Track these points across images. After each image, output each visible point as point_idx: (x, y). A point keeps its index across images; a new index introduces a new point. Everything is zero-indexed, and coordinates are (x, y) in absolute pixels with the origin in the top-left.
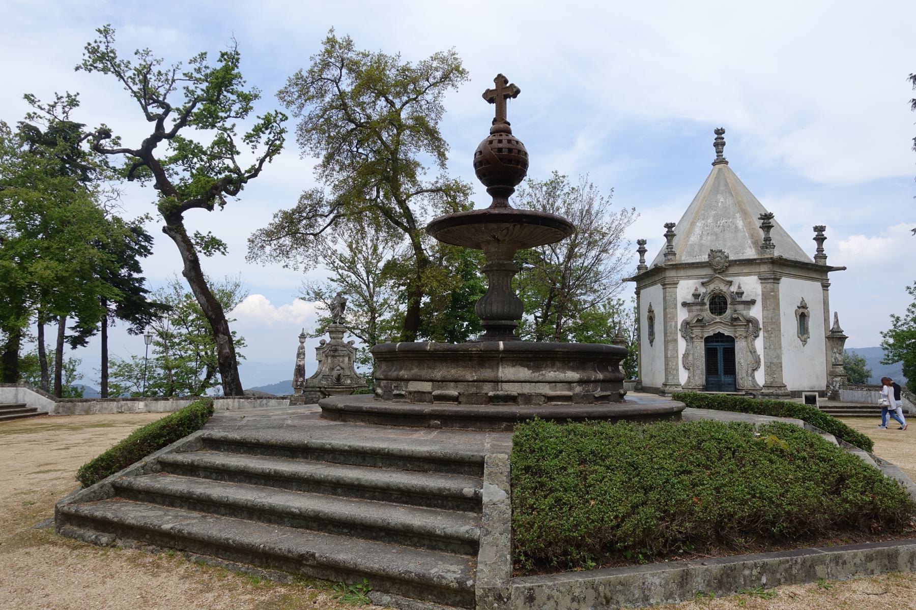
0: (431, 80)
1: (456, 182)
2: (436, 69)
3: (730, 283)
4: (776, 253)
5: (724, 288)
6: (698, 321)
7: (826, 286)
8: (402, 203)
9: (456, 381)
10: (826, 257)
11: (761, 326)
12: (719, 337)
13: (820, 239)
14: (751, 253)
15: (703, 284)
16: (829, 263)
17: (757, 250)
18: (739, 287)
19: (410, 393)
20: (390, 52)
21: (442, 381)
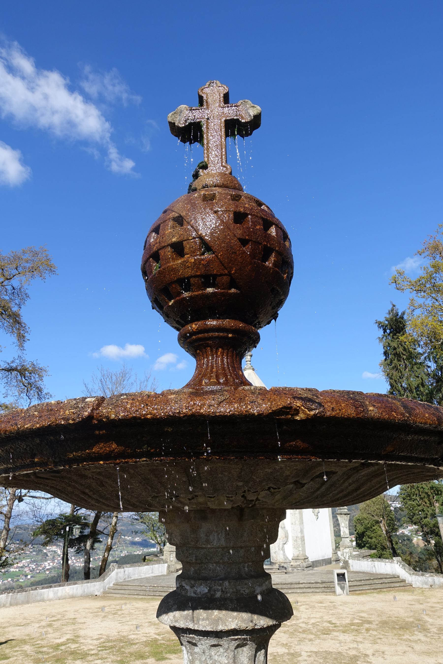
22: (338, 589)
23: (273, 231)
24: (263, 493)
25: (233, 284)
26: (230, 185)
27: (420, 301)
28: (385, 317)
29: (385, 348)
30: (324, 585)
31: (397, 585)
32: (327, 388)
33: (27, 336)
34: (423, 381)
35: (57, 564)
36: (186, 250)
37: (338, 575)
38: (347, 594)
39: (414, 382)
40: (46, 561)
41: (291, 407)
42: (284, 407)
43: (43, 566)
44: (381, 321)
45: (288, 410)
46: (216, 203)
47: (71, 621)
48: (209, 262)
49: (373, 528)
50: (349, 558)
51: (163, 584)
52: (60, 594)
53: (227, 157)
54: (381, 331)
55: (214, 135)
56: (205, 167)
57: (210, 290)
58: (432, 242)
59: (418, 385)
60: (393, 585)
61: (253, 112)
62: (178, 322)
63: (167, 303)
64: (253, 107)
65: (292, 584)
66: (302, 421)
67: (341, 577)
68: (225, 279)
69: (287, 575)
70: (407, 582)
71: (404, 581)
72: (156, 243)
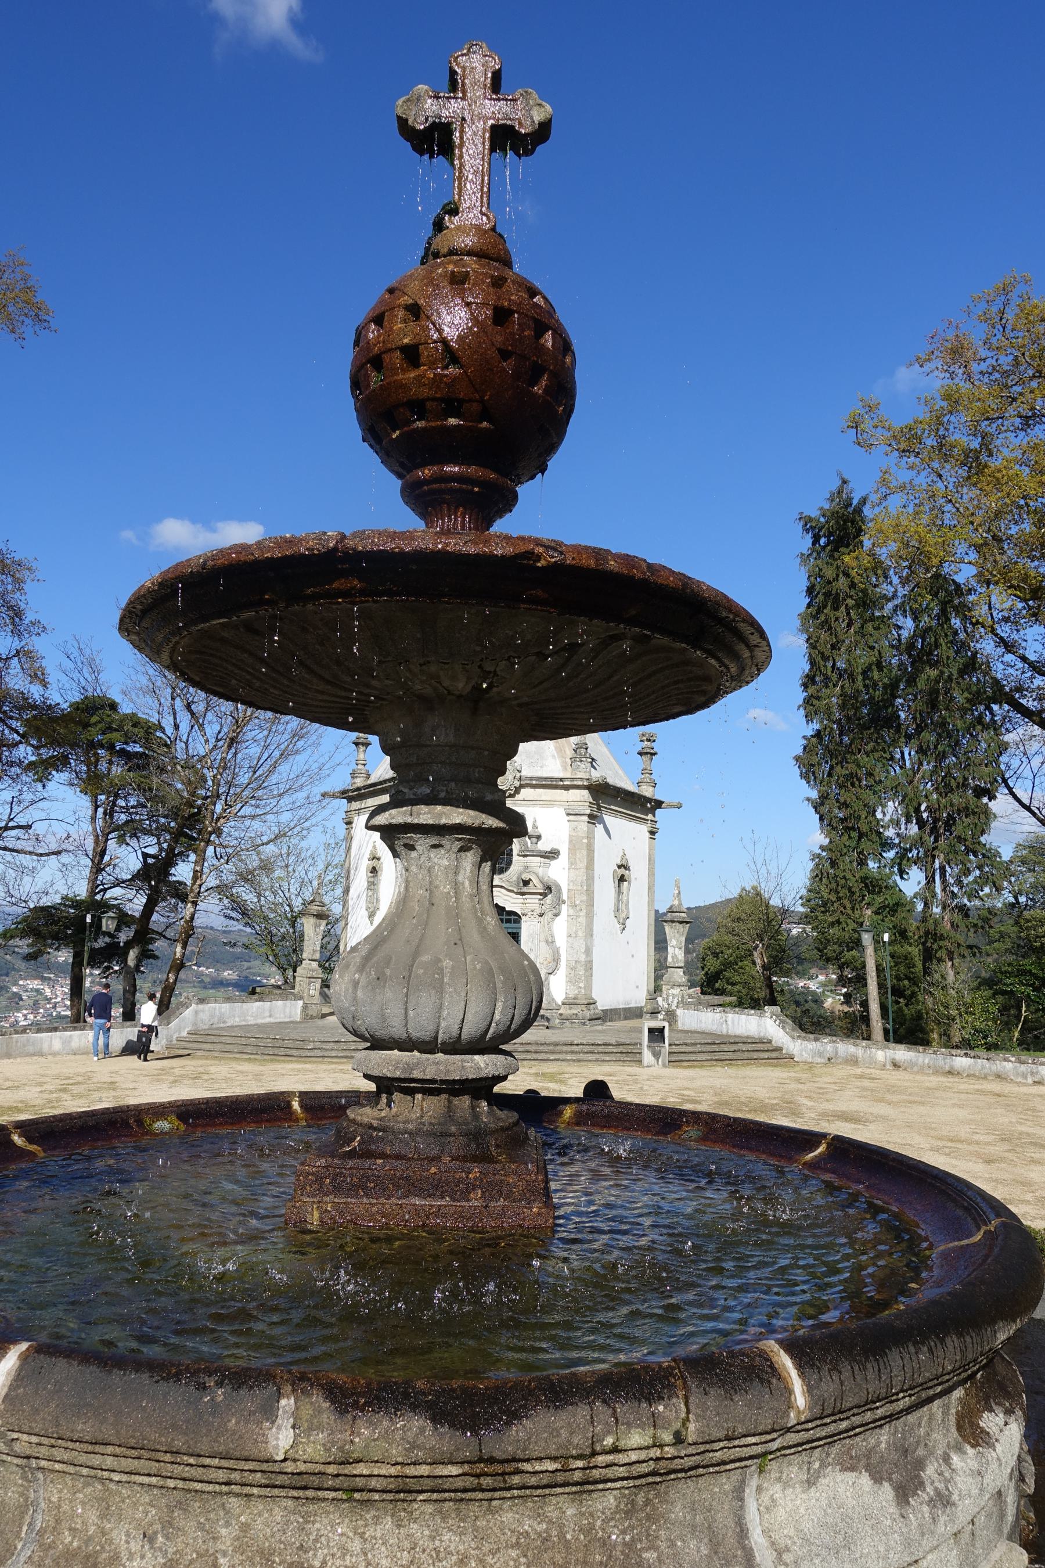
11: (565, 897)
22: (648, 1056)
23: (548, 340)
25: (485, 415)
26: (493, 252)
27: (903, 476)
28: (821, 509)
29: (812, 579)
30: (621, 1049)
31: (766, 1055)
32: (574, 543)
34: (881, 657)
35: (44, 1016)
36: (423, 360)
37: (651, 1031)
38: (664, 1065)
39: (863, 658)
40: (18, 1010)
41: (533, 553)
42: (526, 552)
43: (12, 1019)
44: (813, 516)
45: (530, 555)
46: (470, 289)
47: (106, 1086)
48: (455, 379)
49: (740, 964)
50: (677, 1007)
51: (293, 1036)
52: (75, 1044)
53: (490, 195)
54: (809, 539)
55: (473, 148)
56: (454, 211)
57: (453, 421)
58: (951, 335)
59: (870, 665)
60: (755, 1055)
61: (538, 116)
62: (402, 465)
63: (390, 435)
64: (540, 105)
65: (557, 1044)
66: (543, 567)
67: (656, 1034)
68: (475, 407)
69: (548, 1031)
70: (784, 1051)
71: (779, 1049)
72: (379, 342)
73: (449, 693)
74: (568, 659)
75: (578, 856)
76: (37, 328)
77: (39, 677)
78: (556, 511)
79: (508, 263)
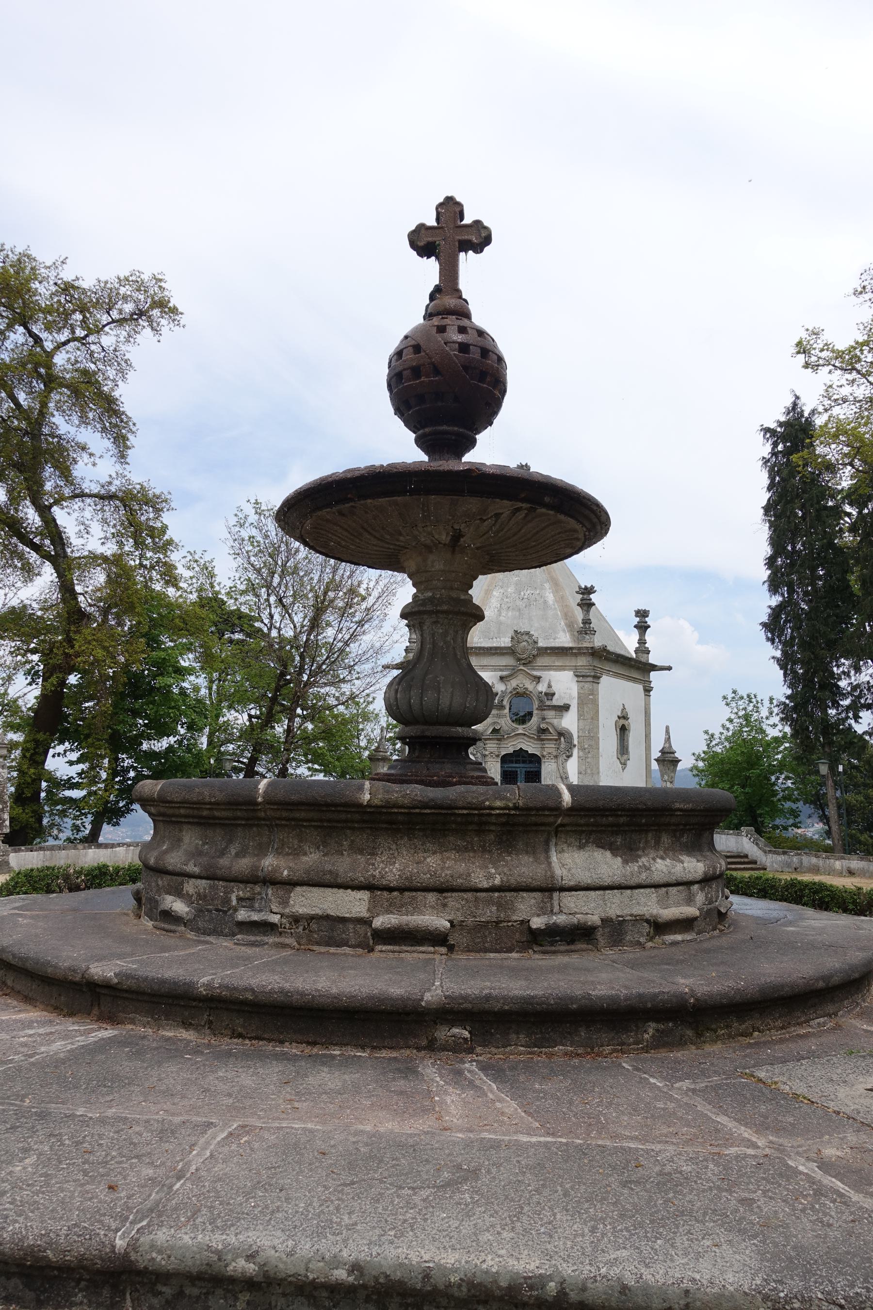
0: (115, 314)
1: (142, 487)
2: (125, 298)
3: (538, 679)
4: (598, 642)
5: (530, 686)
6: (495, 731)
7: (648, 690)
8: (44, 511)
9: (442, 889)
10: (648, 652)
11: (576, 742)
12: (520, 755)
13: (642, 628)
14: (564, 640)
15: (502, 678)
16: (652, 659)
17: (572, 635)
18: (550, 686)
19: (296, 919)
20: (44, 256)
21: (402, 890)
24: (463, 525)
28: (778, 421)
33: (132, 440)
62: (415, 427)
71: (755, 862)
73: (440, 543)
74: (496, 521)
75: (586, 709)
76: (172, 325)
77: (172, 580)
78: (491, 450)
79: (467, 315)
